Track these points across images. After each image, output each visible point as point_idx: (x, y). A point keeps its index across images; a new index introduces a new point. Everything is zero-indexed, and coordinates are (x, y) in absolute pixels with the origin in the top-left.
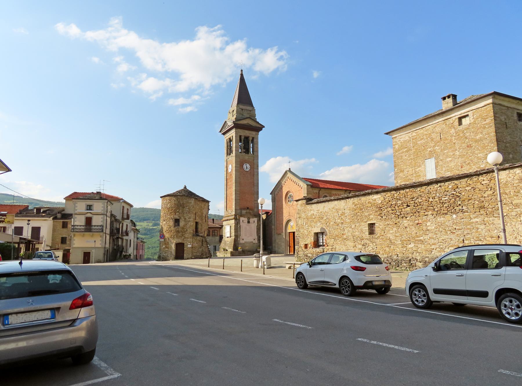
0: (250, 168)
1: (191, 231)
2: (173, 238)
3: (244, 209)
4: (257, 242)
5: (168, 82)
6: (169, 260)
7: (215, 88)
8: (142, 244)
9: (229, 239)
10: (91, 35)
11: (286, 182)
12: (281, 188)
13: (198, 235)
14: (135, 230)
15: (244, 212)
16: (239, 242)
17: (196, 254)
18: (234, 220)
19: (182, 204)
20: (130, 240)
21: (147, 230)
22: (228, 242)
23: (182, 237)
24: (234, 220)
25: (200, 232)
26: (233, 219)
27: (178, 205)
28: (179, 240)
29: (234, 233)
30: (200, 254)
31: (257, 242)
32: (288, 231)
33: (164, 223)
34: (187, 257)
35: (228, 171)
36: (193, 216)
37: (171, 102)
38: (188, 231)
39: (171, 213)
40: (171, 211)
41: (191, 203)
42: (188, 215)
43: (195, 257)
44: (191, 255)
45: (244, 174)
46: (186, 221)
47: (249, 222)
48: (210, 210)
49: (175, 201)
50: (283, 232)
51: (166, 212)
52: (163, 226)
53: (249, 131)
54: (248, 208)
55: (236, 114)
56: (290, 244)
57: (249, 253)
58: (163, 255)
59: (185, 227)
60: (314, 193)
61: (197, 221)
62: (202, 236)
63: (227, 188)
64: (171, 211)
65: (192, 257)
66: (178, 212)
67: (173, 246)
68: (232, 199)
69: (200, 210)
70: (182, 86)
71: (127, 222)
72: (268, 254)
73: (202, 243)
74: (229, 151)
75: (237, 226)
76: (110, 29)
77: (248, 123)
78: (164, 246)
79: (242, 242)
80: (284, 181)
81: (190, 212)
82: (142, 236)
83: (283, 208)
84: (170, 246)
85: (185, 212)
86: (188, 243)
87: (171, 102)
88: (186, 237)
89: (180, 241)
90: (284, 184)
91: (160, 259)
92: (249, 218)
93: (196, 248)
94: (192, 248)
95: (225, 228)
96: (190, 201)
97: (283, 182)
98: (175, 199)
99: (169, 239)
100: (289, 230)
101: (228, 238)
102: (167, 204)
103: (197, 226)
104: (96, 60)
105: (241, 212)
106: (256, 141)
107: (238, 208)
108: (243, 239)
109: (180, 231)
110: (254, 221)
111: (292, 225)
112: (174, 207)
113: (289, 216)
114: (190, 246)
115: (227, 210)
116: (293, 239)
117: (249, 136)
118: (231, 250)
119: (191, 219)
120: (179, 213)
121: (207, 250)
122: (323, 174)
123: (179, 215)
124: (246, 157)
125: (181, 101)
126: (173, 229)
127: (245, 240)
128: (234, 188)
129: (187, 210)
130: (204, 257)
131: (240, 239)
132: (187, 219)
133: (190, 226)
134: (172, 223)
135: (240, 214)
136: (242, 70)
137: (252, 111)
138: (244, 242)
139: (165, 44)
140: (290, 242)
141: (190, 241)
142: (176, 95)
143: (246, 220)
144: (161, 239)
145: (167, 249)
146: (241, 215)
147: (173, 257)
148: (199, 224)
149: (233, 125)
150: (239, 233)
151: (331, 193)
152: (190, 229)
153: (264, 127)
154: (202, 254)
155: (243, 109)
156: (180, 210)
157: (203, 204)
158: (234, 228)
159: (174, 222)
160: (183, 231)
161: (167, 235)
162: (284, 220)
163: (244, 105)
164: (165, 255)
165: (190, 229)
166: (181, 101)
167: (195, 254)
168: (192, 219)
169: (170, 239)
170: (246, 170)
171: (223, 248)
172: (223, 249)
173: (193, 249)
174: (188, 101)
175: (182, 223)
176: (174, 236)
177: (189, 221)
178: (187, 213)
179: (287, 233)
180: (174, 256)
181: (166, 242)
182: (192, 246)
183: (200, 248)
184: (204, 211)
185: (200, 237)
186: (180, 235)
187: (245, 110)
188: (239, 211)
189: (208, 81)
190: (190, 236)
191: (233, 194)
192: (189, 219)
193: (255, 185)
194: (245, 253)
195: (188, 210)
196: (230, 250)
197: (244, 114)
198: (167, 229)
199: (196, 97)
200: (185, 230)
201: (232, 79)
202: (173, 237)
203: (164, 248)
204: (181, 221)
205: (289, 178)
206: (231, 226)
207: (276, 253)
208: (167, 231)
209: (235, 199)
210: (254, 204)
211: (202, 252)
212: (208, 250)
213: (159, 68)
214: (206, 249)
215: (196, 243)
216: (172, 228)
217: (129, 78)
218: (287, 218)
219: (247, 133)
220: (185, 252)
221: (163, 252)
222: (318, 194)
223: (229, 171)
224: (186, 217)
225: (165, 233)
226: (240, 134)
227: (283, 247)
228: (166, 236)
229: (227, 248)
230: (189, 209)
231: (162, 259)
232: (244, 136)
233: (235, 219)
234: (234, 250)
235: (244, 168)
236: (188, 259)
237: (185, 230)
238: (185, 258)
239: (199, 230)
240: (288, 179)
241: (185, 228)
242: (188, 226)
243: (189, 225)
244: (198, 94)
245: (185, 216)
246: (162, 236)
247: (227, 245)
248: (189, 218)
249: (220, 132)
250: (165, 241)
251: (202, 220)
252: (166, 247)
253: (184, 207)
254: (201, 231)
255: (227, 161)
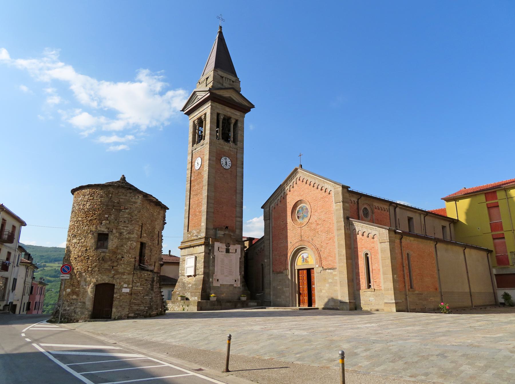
0: (230, 165)
1: (132, 260)
2: (92, 273)
3: (221, 229)
4: (239, 286)
5: (103, 119)
6: (77, 321)
7: (149, 130)
8: (39, 286)
9: (192, 280)
10: (22, 63)
11: (296, 183)
12: (284, 198)
13: (143, 269)
14: (29, 265)
15: (220, 233)
16: (211, 285)
17: (138, 308)
18: (203, 246)
19: (115, 204)
20: (15, 280)
21: (57, 273)
22: (190, 285)
23: (110, 272)
24: (203, 246)
25: (147, 262)
26: (201, 245)
27: (107, 205)
28: (105, 277)
29: (203, 269)
30: (147, 308)
31: (239, 286)
32: (297, 268)
33: (75, 241)
34: (119, 314)
35: (193, 168)
36: (137, 229)
37: (104, 139)
38: (126, 258)
39: (91, 220)
40: (92, 216)
41: (135, 203)
42: (127, 227)
43: (135, 314)
44: (128, 310)
45: (221, 173)
46: (123, 239)
47: (228, 251)
48: (166, 223)
49: (101, 197)
50: (286, 269)
51: (80, 219)
52: (71, 248)
53: (231, 109)
54: (227, 227)
55: (213, 82)
56: (301, 289)
57: (228, 304)
58: (65, 310)
59: (119, 251)
60: (352, 202)
61: (144, 240)
62: (151, 271)
63: (191, 196)
64: (92, 216)
65: (128, 314)
66: (107, 219)
67: (90, 290)
68: (200, 212)
69: (150, 221)
70: (117, 125)
71: (9, 247)
72: (257, 306)
73: (152, 286)
74: (198, 138)
75: (209, 257)
76: (45, 59)
77: (230, 97)
78: (69, 290)
79: (215, 284)
80: (290, 185)
81: (132, 221)
82: (51, 278)
83: (288, 229)
84: (82, 290)
85: (121, 219)
86: (122, 283)
87: (104, 139)
88: (120, 271)
89: (106, 279)
90: (290, 191)
91: (57, 317)
92: (228, 244)
93: (139, 294)
94: (131, 294)
95: (185, 260)
96: (133, 200)
97: (288, 187)
98: (101, 192)
99: (81, 274)
100: (299, 264)
101: (190, 278)
102: (85, 203)
103: (143, 251)
104: (24, 88)
105: (216, 235)
106: (241, 125)
107: (211, 227)
108: (218, 280)
109: (108, 257)
110: (236, 250)
111: (305, 257)
112: (99, 209)
113: (302, 242)
114: (128, 290)
115: (188, 231)
116: (306, 281)
117: (231, 116)
118: (196, 298)
119: (133, 234)
120: (108, 222)
121: (159, 298)
122: (251, 220)
123: (108, 226)
124: (227, 147)
125: (114, 139)
126: (92, 254)
127: (221, 282)
128: (205, 193)
129: (127, 216)
130: (154, 313)
131: (212, 279)
132: (125, 233)
133: (130, 248)
134: (90, 241)
135: (214, 237)
136: (221, 27)
137: (236, 82)
138: (219, 285)
139: (103, 81)
140: (301, 286)
141: (127, 280)
142: (109, 133)
143: (223, 246)
144: (64, 275)
145: (74, 297)
146: (216, 239)
147: (87, 313)
148: (147, 248)
149: (209, 94)
150: (211, 268)
151: (373, 205)
152: (130, 256)
153: (253, 106)
154: (150, 308)
155: (223, 77)
156: (110, 214)
157: (157, 210)
158: (203, 260)
159: (96, 240)
160: (113, 258)
161: (77, 267)
162: (289, 248)
163: (224, 72)
164: (68, 308)
165: (130, 256)
166: (114, 139)
167: (136, 307)
168: (134, 236)
169: (84, 274)
170: (225, 167)
171: (179, 294)
172: (181, 296)
173: (134, 296)
174: (123, 140)
175: (112, 243)
176: (93, 268)
177: (129, 239)
178: (125, 222)
179: (295, 270)
180: (89, 311)
181: (75, 281)
182: (131, 291)
183: (147, 295)
184: (156, 223)
185: (149, 273)
186: (106, 266)
187: (227, 79)
188: (212, 232)
189: (144, 121)
190: (129, 269)
191: (203, 203)
192: (130, 235)
193: (238, 191)
194: (221, 305)
195: (129, 216)
196: (195, 299)
197: (224, 84)
198: (80, 254)
199: (131, 137)
200: (120, 256)
201: (169, 123)
202: (92, 271)
203: (69, 294)
204: (111, 237)
205: (301, 180)
206: (196, 258)
207: (272, 304)
208: (78, 259)
209: (207, 212)
210: (235, 221)
211: (150, 304)
212: (160, 299)
213: (94, 104)
214: (157, 297)
215: (139, 284)
216: (91, 253)
217: (60, 111)
218: (297, 245)
219: (228, 112)
220: (115, 303)
221: (65, 302)
222: (356, 203)
223: (197, 167)
224: (124, 229)
225: (73, 263)
226: (219, 112)
227: (287, 294)
228: (76, 268)
229: (188, 295)
230: (129, 214)
231: (61, 319)
232: (224, 115)
233: (206, 244)
234: (202, 298)
235: (223, 164)
236: (120, 318)
237: (120, 256)
238: (113, 317)
239: (146, 258)
240: (298, 182)
241: (120, 253)
242: (126, 248)
243: (128, 248)
244: (132, 134)
245: (121, 227)
246: (66, 269)
247: (189, 290)
248: (129, 233)
249: (183, 110)
250: (71, 278)
251: (152, 239)
252: (73, 292)
253: (120, 210)
254: (149, 261)
255: (192, 154)
